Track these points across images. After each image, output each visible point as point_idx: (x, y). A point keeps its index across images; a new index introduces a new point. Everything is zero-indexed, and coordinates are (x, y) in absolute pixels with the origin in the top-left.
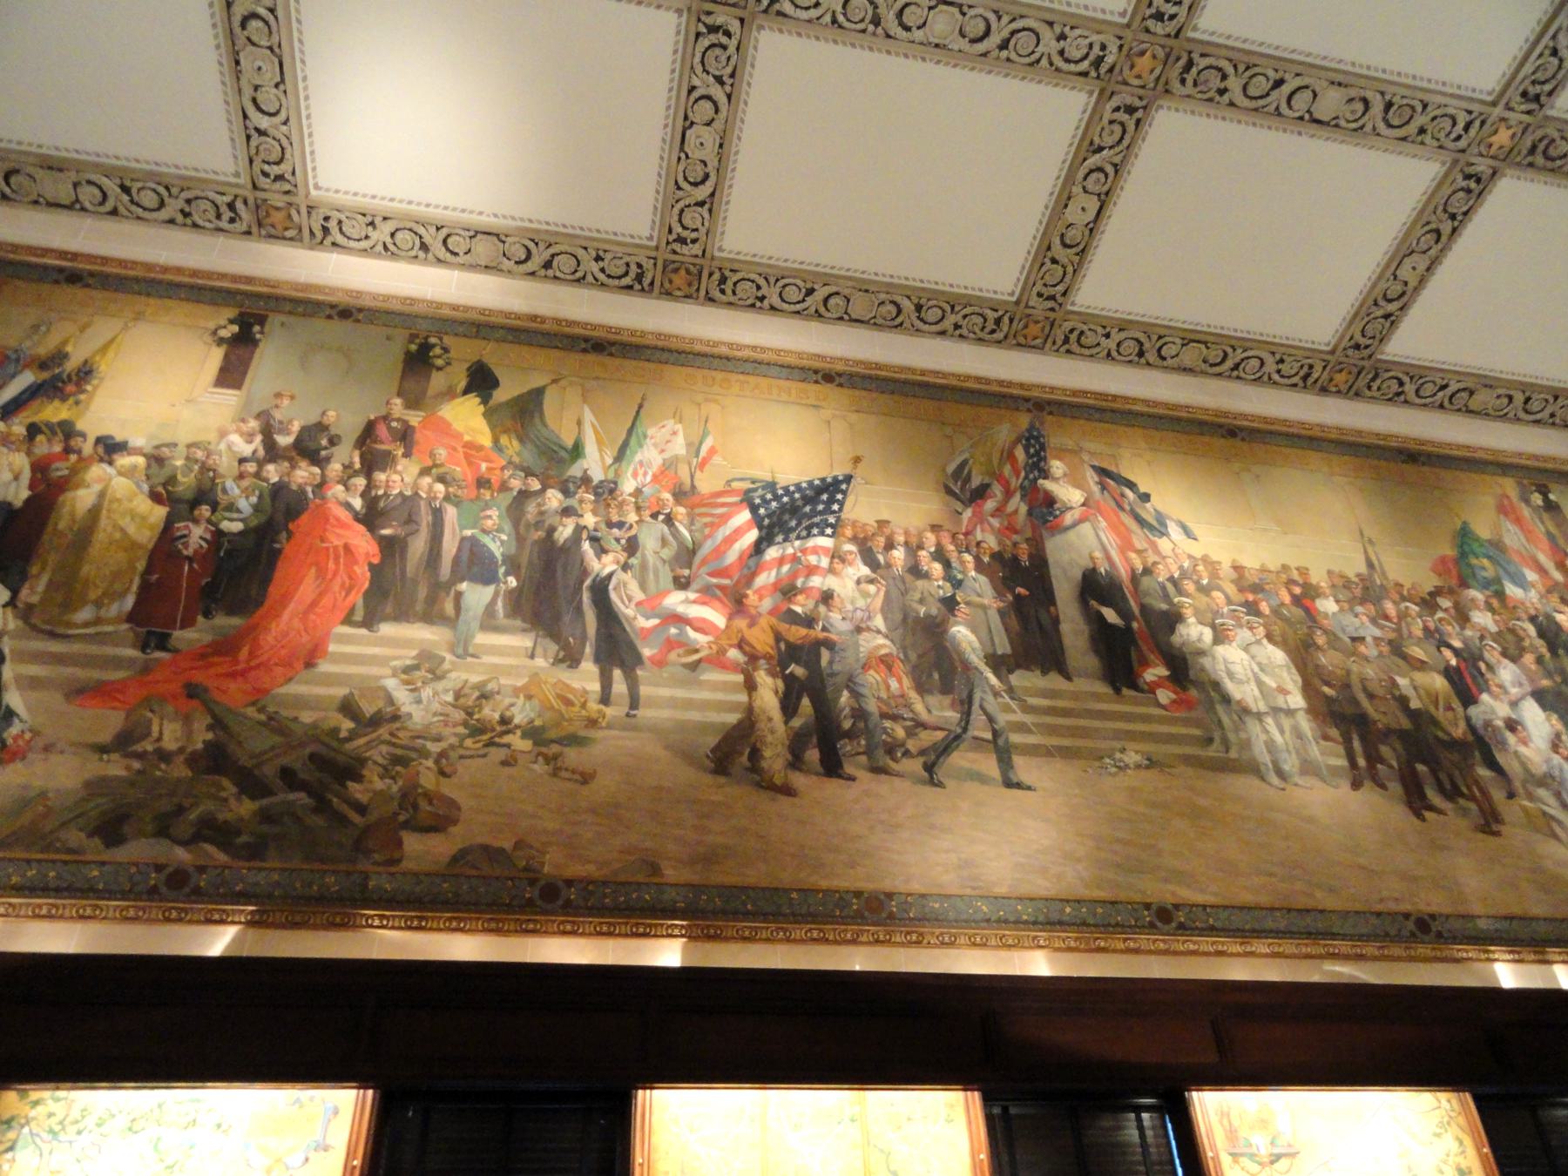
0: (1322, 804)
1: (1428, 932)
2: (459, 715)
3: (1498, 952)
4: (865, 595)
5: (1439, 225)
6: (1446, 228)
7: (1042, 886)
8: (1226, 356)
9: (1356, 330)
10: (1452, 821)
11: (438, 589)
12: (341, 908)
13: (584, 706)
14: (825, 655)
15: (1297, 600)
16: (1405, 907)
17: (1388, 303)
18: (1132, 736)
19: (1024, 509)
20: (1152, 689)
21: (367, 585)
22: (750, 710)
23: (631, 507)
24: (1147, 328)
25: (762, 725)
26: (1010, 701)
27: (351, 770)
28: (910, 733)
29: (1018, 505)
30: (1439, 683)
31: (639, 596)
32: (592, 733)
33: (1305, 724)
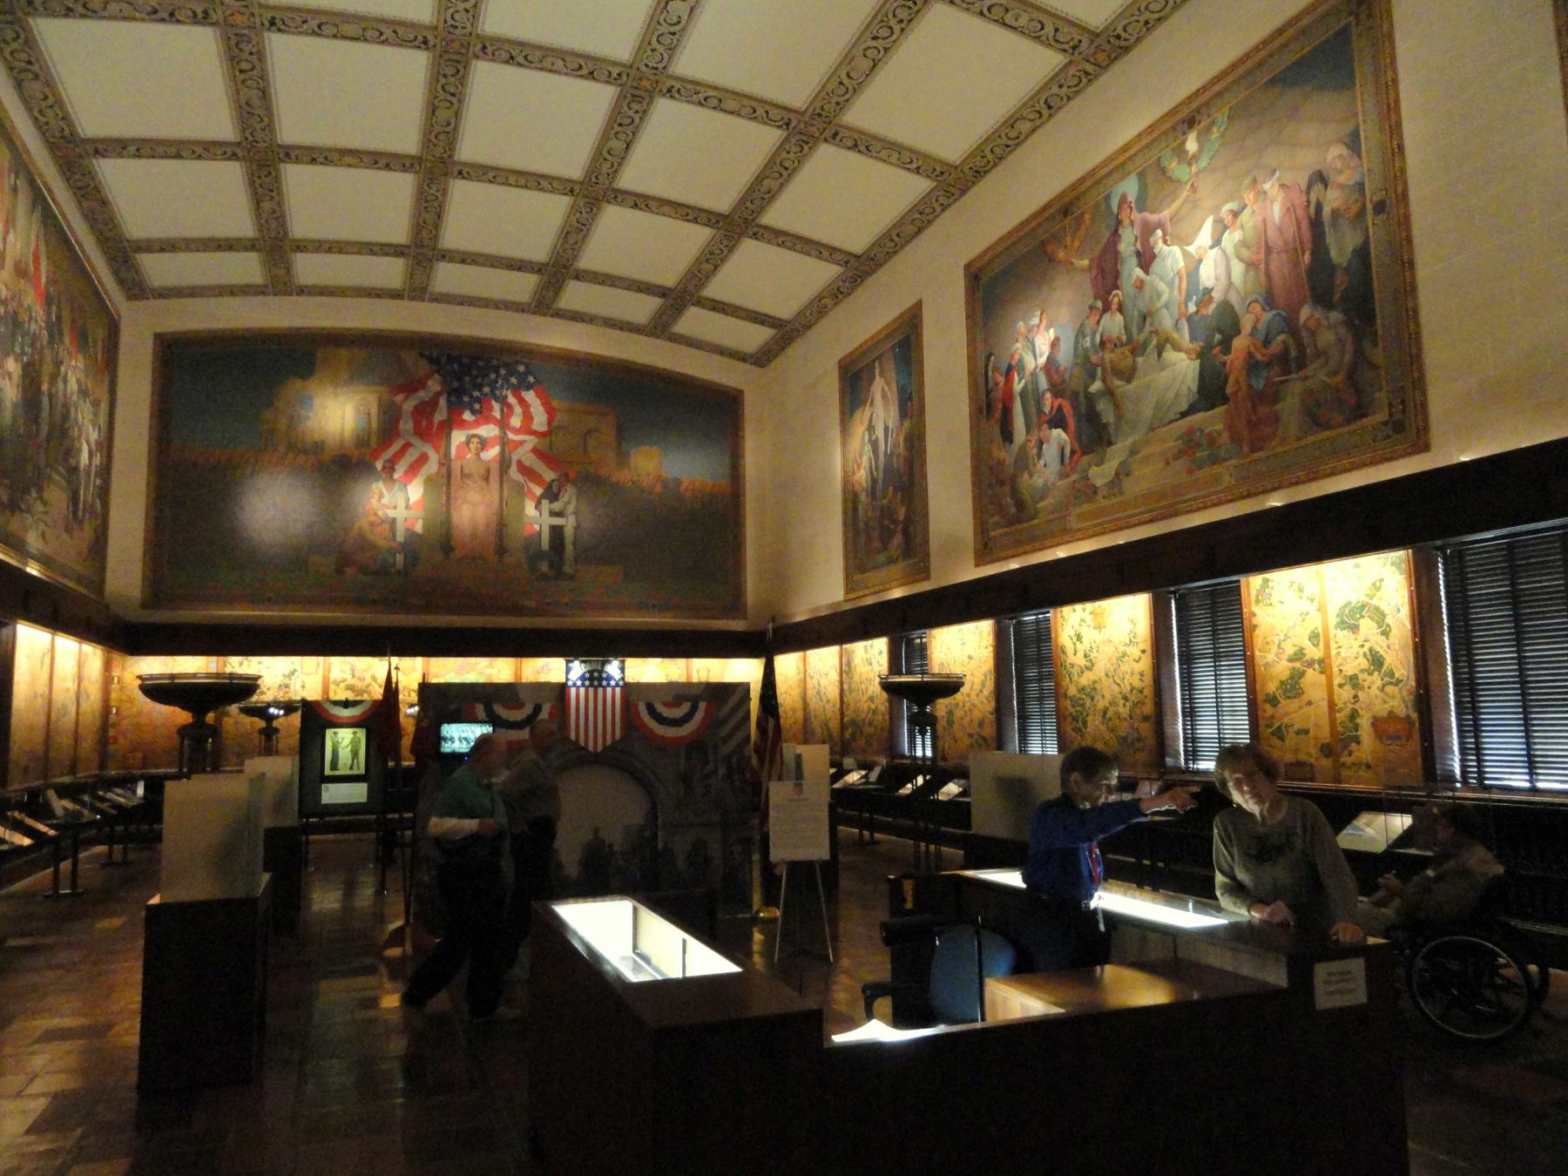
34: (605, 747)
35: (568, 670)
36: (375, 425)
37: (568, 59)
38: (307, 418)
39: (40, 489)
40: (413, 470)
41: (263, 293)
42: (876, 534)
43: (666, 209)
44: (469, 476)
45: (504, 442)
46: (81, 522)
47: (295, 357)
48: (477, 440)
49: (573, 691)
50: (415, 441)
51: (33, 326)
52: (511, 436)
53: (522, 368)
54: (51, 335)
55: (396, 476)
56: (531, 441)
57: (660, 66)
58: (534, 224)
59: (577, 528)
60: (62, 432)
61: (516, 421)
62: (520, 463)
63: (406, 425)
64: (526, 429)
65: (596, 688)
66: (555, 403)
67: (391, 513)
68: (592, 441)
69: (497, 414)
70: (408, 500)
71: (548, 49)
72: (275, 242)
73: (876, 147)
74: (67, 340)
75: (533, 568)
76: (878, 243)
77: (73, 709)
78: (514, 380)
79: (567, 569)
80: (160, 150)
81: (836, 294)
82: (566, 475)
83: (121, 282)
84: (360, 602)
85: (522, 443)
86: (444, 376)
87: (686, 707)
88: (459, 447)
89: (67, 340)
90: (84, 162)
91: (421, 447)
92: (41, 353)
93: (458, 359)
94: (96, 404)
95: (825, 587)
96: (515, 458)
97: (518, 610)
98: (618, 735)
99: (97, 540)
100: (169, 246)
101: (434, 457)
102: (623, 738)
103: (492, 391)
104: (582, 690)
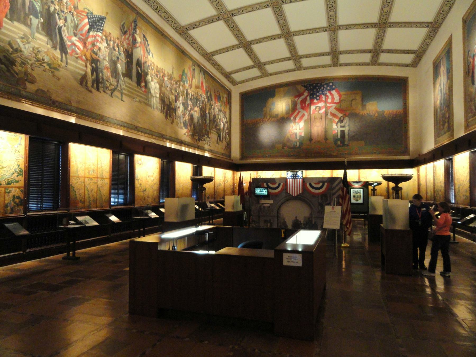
0: (157, 113)
1: (162, 137)
2: (34, 55)
3: (168, 141)
4: (106, 51)
5: (210, 20)
6: (211, 21)
7: (123, 120)
8: (168, 18)
9: (188, 27)
10: (169, 121)
11: (26, 15)
12: (18, 97)
13: (58, 61)
14: (98, 63)
15: (163, 76)
16: (161, 133)
17: (195, 25)
18: (138, 95)
19: (132, 40)
20: (141, 87)
21: (9, 7)
22: (86, 72)
23: (65, 7)
24: (161, 6)
25: (88, 76)
26: (124, 82)
27: (13, 63)
28: (110, 86)
29: (131, 38)
30: (174, 98)
31: (67, 35)
32: (59, 68)
33: (158, 100)
35: (287, 174)
36: (290, 108)
39: (208, 135)
40: (301, 118)
41: (262, 77)
42: (441, 123)
43: (357, 27)
44: (316, 118)
45: (326, 107)
47: (268, 93)
48: (318, 108)
49: (288, 180)
50: (301, 110)
51: (202, 99)
52: (328, 105)
53: (331, 84)
54: (208, 100)
55: (296, 121)
56: (334, 106)
58: (367, 38)
59: (349, 131)
60: (214, 121)
61: (329, 100)
62: (331, 113)
63: (299, 106)
64: (333, 102)
66: (342, 93)
67: (295, 131)
68: (353, 103)
69: (324, 99)
72: (295, 56)
74: (214, 100)
76: (437, 16)
78: (329, 88)
79: (346, 143)
80: (224, 51)
81: (430, 37)
84: (288, 156)
85: (332, 106)
86: (312, 89)
87: (321, 184)
89: (214, 100)
91: (303, 112)
93: (312, 85)
94: (225, 113)
95: (430, 145)
96: (329, 111)
97: (331, 156)
98: (301, 192)
99: (228, 145)
100: (236, 71)
102: (302, 192)
103: (322, 93)
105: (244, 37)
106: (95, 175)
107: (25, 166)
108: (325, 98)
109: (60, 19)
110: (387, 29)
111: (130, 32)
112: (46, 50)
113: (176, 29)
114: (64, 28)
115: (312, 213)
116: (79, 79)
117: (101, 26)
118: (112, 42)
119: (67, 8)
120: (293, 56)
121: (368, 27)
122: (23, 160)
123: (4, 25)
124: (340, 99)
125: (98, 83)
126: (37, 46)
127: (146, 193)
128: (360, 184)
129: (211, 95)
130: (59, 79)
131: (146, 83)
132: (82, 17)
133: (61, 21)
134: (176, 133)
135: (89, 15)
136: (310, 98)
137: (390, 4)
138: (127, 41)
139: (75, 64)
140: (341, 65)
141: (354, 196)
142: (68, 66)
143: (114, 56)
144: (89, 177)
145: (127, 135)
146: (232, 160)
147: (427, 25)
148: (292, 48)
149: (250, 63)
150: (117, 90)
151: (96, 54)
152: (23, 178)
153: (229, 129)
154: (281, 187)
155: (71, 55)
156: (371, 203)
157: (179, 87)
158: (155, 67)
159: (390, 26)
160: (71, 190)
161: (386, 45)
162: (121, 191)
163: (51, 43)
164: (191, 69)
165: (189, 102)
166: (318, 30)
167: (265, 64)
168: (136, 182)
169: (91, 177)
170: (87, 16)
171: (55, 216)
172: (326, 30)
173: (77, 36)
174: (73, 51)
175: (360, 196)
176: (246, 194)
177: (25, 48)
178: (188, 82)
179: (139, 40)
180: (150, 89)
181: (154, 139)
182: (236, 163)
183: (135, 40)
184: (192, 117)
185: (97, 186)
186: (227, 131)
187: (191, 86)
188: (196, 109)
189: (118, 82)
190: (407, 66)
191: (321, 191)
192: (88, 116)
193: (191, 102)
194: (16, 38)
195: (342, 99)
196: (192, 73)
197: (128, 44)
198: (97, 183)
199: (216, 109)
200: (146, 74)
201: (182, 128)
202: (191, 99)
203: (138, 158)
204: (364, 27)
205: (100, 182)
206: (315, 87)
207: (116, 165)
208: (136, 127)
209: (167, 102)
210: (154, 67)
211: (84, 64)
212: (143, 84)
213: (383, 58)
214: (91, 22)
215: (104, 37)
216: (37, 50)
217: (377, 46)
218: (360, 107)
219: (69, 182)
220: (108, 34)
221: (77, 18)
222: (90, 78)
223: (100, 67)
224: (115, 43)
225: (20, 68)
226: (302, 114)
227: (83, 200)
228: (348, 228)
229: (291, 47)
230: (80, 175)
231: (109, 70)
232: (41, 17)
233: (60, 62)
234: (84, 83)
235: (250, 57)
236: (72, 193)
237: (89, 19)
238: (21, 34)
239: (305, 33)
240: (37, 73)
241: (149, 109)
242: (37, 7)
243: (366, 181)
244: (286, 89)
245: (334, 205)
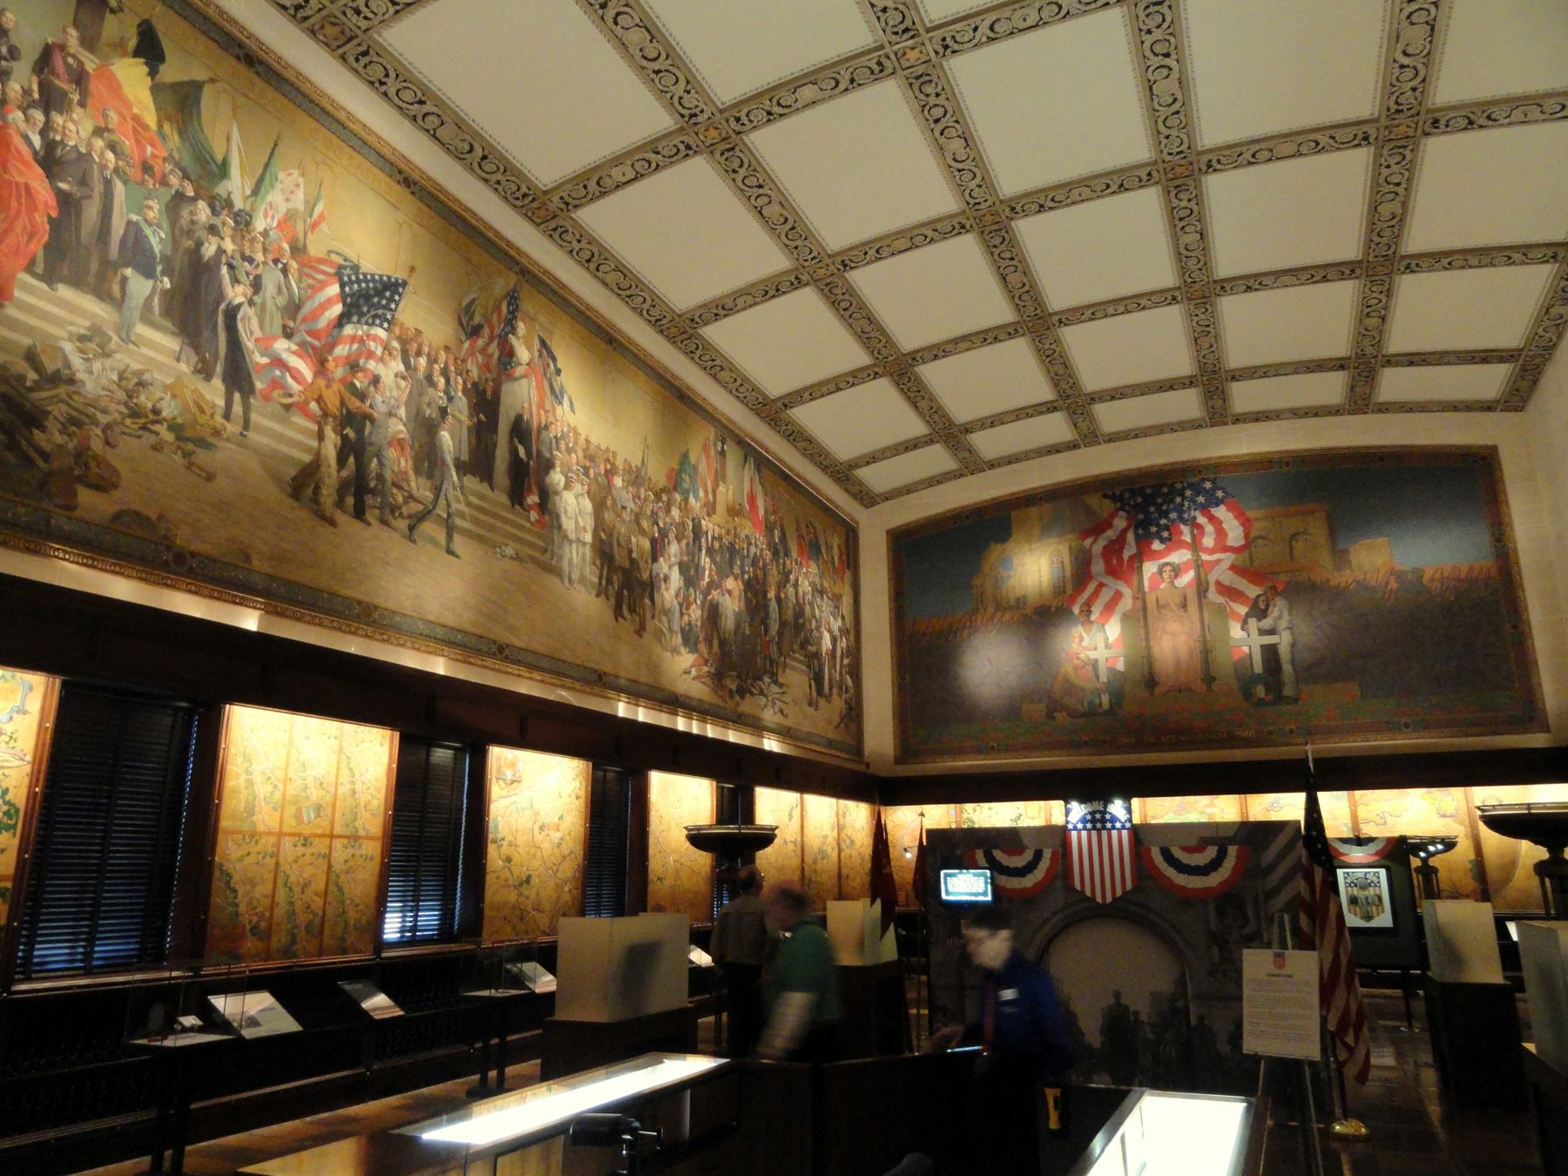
0: (581, 597)
1: (601, 681)
2: (122, 396)
3: (624, 697)
4: (399, 387)
5: (770, 289)
6: (772, 292)
7: (451, 620)
8: (629, 287)
10: (627, 625)
12: (37, 537)
13: (212, 415)
17: (722, 308)
19: (497, 354)
21: (46, 238)
22: (318, 454)
23: (259, 246)
25: (323, 469)
26: (461, 492)
27: (35, 419)
28: (406, 502)
29: (494, 349)
30: (647, 544)
31: (258, 334)
32: (214, 441)
33: (588, 551)
34: (1115, 899)
35: (1067, 812)
36: (1068, 573)
37: (1093, 183)
38: (1009, 577)
40: (1109, 608)
45: (1198, 565)
46: (828, 699)
47: (990, 525)
48: (1170, 568)
49: (1074, 834)
50: (1108, 580)
51: (753, 550)
52: (1205, 557)
54: (776, 553)
55: (1093, 618)
56: (1228, 558)
57: (1184, 147)
58: (1326, 321)
59: (1293, 646)
60: (797, 628)
61: (1208, 541)
62: (1218, 584)
63: (1098, 567)
65: (1099, 831)
66: (1251, 514)
67: (1093, 655)
68: (1299, 546)
69: (1187, 538)
70: (1107, 639)
71: (1070, 183)
72: (1071, 398)
73: (1498, 113)
74: (794, 554)
75: (1247, 693)
77: (835, 854)
78: (1201, 499)
79: (1288, 691)
80: (824, 389)
82: (1274, 588)
83: (854, 496)
84: (1072, 746)
85: (1218, 562)
86: (1142, 505)
87: (1211, 852)
88: (1152, 578)
89: (794, 554)
90: (783, 416)
92: (764, 569)
93: (1141, 492)
94: (837, 598)
96: (1212, 578)
97: (1232, 741)
98: (1129, 886)
99: (850, 709)
100: (872, 458)
101: (1127, 592)
102: (1135, 888)
104: (1084, 833)
105: (889, 340)
106: (324, 826)
107: (31, 795)
108: (1193, 537)
109: (235, 281)
110: (1397, 278)
111: (492, 331)
112: (169, 381)
113: (657, 324)
114: (246, 311)
115: (1183, 974)
116: (287, 478)
117: (387, 307)
118: (423, 361)
119: (265, 250)
120: (1063, 396)
121: (1325, 279)
122: (28, 769)
123: (17, 293)
124: (1246, 536)
125: (362, 492)
126: (135, 366)
127: (531, 893)
128: (1373, 847)
129: (783, 539)
130: (210, 477)
131: (546, 495)
132: (320, 277)
133: (240, 289)
134: (654, 667)
135: (345, 273)
136: (1138, 538)
137: (1400, 190)
138: (480, 358)
139: (277, 427)
140: (1238, 420)
141: (1353, 901)
142: (249, 434)
143: (429, 405)
144: (299, 835)
145: (461, 676)
146: (868, 765)
147: (1550, 253)
148: (1061, 370)
149: (918, 428)
150: (432, 518)
151: (362, 396)
152: (16, 841)
153: (855, 652)
154: (1044, 864)
155: (267, 398)
156: (1438, 930)
157: (668, 511)
158: (582, 441)
159: (1408, 267)
160: (217, 884)
161: (1398, 341)
162: (429, 884)
163: (194, 358)
164: (713, 453)
165: (705, 561)
166: (1144, 302)
167: (968, 429)
168: (492, 850)
169: (306, 832)
170: (339, 274)
171: (121, 993)
172: (1174, 298)
173: (296, 338)
174: (276, 384)
175: (1380, 898)
176: (901, 895)
177: (91, 372)
178: (701, 494)
179: (523, 354)
180: (558, 516)
181: (563, 687)
182: (885, 774)
183: (508, 354)
184: (713, 614)
185: (330, 867)
186: (846, 661)
187: (711, 509)
188: (730, 583)
189: (437, 490)
190: (1488, 407)
191: (1214, 880)
192: (313, 606)
193: (713, 561)
194: (58, 338)
195: (1254, 534)
196: (715, 465)
197: (486, 367)
198: (328, 857)
199: (805, 586)
200: (549, 465)
201: (675, 651)
202: (710, 551)
203: (499, 756)
204: (1312, 280)
205: (340, 853)
206: (1149, 500)
207: (410, 783)
208: (501, 649)
209: (620, 558)
210: (576, 443)
211: (316, 428)
212: (533, 499)
213: (1393, 384)
214: (352, 295)
215: (395, 344)
216: (135, 380)
217: (1367, 342)
218: (1326, 560)
219: (213, 854)
220: (411, 333)
221: (299, 281)
222: (332, 474)
223: (373, 439)
224: (436, 361)
225: (59, 438)
226: (1112, 593)
227: (263, 925)
228: (1351, 1050)
229: (1057, 365)
230: (261, 828)
231: (408, 449)
232: (164, 273)
233: (219, 419)
234: (309, 491)
235: (915, 406)
236: (217, 899)
237: (342, 286)
238: (83, 325)
239: (1098, 314)
240: (127, 455)
241: (551, 581)
242: (154, 241)
243: (1396, 834)
244: (1047, 508)
245: (1284, 946)
